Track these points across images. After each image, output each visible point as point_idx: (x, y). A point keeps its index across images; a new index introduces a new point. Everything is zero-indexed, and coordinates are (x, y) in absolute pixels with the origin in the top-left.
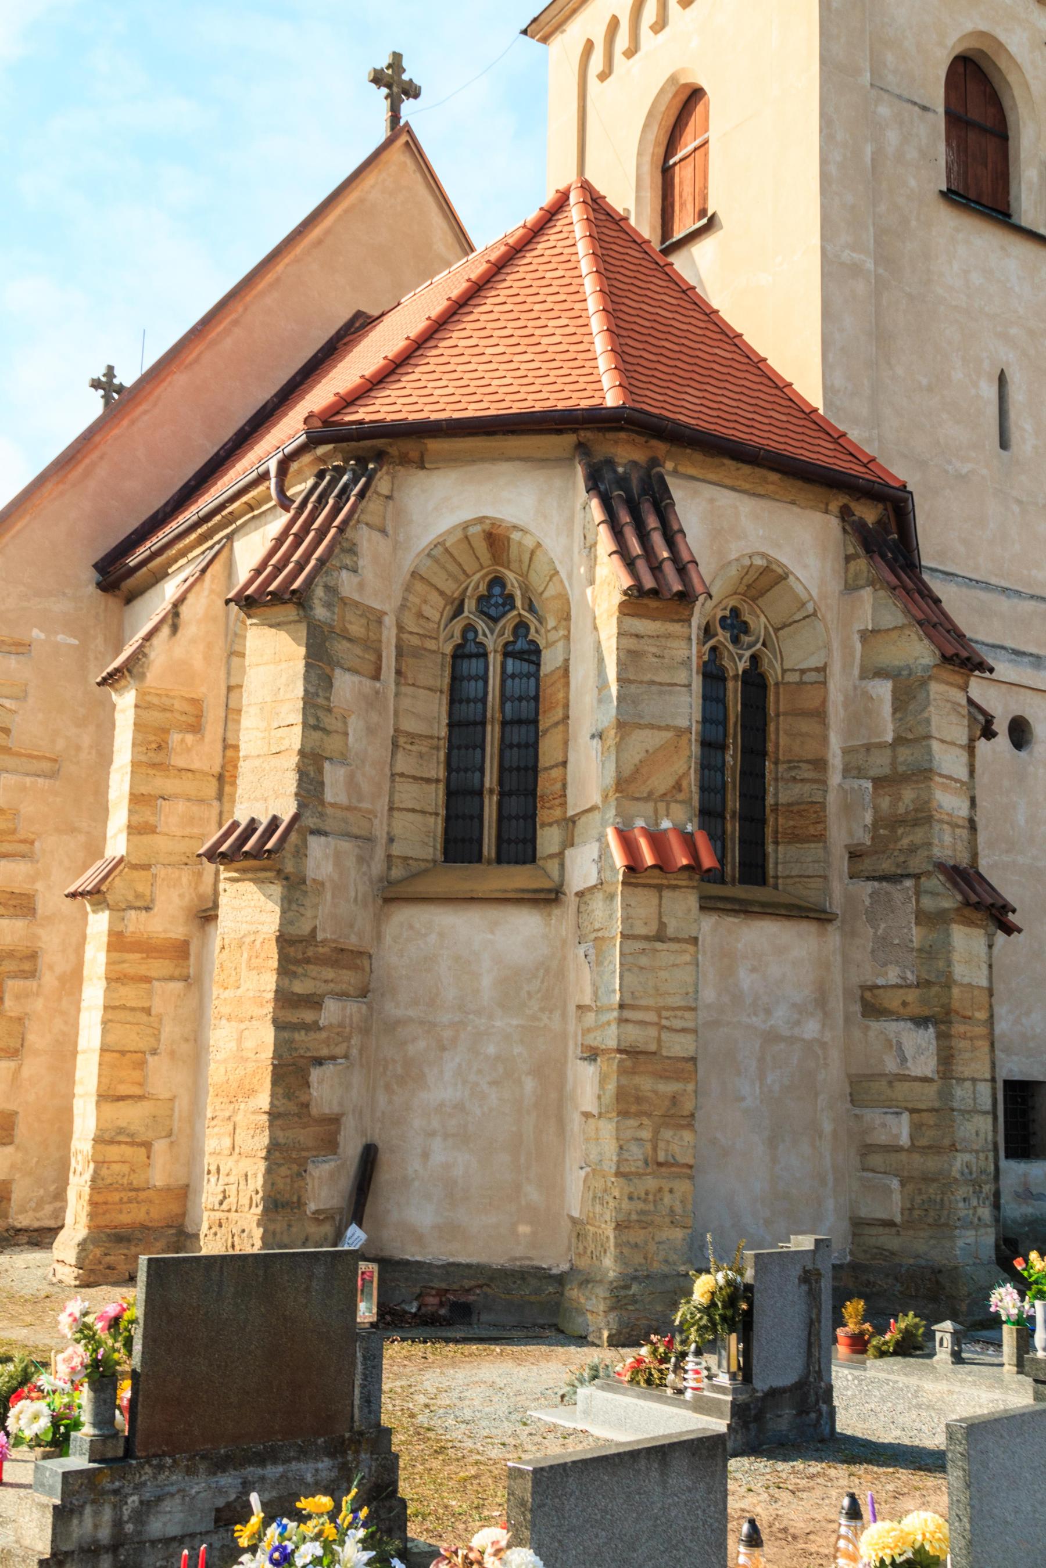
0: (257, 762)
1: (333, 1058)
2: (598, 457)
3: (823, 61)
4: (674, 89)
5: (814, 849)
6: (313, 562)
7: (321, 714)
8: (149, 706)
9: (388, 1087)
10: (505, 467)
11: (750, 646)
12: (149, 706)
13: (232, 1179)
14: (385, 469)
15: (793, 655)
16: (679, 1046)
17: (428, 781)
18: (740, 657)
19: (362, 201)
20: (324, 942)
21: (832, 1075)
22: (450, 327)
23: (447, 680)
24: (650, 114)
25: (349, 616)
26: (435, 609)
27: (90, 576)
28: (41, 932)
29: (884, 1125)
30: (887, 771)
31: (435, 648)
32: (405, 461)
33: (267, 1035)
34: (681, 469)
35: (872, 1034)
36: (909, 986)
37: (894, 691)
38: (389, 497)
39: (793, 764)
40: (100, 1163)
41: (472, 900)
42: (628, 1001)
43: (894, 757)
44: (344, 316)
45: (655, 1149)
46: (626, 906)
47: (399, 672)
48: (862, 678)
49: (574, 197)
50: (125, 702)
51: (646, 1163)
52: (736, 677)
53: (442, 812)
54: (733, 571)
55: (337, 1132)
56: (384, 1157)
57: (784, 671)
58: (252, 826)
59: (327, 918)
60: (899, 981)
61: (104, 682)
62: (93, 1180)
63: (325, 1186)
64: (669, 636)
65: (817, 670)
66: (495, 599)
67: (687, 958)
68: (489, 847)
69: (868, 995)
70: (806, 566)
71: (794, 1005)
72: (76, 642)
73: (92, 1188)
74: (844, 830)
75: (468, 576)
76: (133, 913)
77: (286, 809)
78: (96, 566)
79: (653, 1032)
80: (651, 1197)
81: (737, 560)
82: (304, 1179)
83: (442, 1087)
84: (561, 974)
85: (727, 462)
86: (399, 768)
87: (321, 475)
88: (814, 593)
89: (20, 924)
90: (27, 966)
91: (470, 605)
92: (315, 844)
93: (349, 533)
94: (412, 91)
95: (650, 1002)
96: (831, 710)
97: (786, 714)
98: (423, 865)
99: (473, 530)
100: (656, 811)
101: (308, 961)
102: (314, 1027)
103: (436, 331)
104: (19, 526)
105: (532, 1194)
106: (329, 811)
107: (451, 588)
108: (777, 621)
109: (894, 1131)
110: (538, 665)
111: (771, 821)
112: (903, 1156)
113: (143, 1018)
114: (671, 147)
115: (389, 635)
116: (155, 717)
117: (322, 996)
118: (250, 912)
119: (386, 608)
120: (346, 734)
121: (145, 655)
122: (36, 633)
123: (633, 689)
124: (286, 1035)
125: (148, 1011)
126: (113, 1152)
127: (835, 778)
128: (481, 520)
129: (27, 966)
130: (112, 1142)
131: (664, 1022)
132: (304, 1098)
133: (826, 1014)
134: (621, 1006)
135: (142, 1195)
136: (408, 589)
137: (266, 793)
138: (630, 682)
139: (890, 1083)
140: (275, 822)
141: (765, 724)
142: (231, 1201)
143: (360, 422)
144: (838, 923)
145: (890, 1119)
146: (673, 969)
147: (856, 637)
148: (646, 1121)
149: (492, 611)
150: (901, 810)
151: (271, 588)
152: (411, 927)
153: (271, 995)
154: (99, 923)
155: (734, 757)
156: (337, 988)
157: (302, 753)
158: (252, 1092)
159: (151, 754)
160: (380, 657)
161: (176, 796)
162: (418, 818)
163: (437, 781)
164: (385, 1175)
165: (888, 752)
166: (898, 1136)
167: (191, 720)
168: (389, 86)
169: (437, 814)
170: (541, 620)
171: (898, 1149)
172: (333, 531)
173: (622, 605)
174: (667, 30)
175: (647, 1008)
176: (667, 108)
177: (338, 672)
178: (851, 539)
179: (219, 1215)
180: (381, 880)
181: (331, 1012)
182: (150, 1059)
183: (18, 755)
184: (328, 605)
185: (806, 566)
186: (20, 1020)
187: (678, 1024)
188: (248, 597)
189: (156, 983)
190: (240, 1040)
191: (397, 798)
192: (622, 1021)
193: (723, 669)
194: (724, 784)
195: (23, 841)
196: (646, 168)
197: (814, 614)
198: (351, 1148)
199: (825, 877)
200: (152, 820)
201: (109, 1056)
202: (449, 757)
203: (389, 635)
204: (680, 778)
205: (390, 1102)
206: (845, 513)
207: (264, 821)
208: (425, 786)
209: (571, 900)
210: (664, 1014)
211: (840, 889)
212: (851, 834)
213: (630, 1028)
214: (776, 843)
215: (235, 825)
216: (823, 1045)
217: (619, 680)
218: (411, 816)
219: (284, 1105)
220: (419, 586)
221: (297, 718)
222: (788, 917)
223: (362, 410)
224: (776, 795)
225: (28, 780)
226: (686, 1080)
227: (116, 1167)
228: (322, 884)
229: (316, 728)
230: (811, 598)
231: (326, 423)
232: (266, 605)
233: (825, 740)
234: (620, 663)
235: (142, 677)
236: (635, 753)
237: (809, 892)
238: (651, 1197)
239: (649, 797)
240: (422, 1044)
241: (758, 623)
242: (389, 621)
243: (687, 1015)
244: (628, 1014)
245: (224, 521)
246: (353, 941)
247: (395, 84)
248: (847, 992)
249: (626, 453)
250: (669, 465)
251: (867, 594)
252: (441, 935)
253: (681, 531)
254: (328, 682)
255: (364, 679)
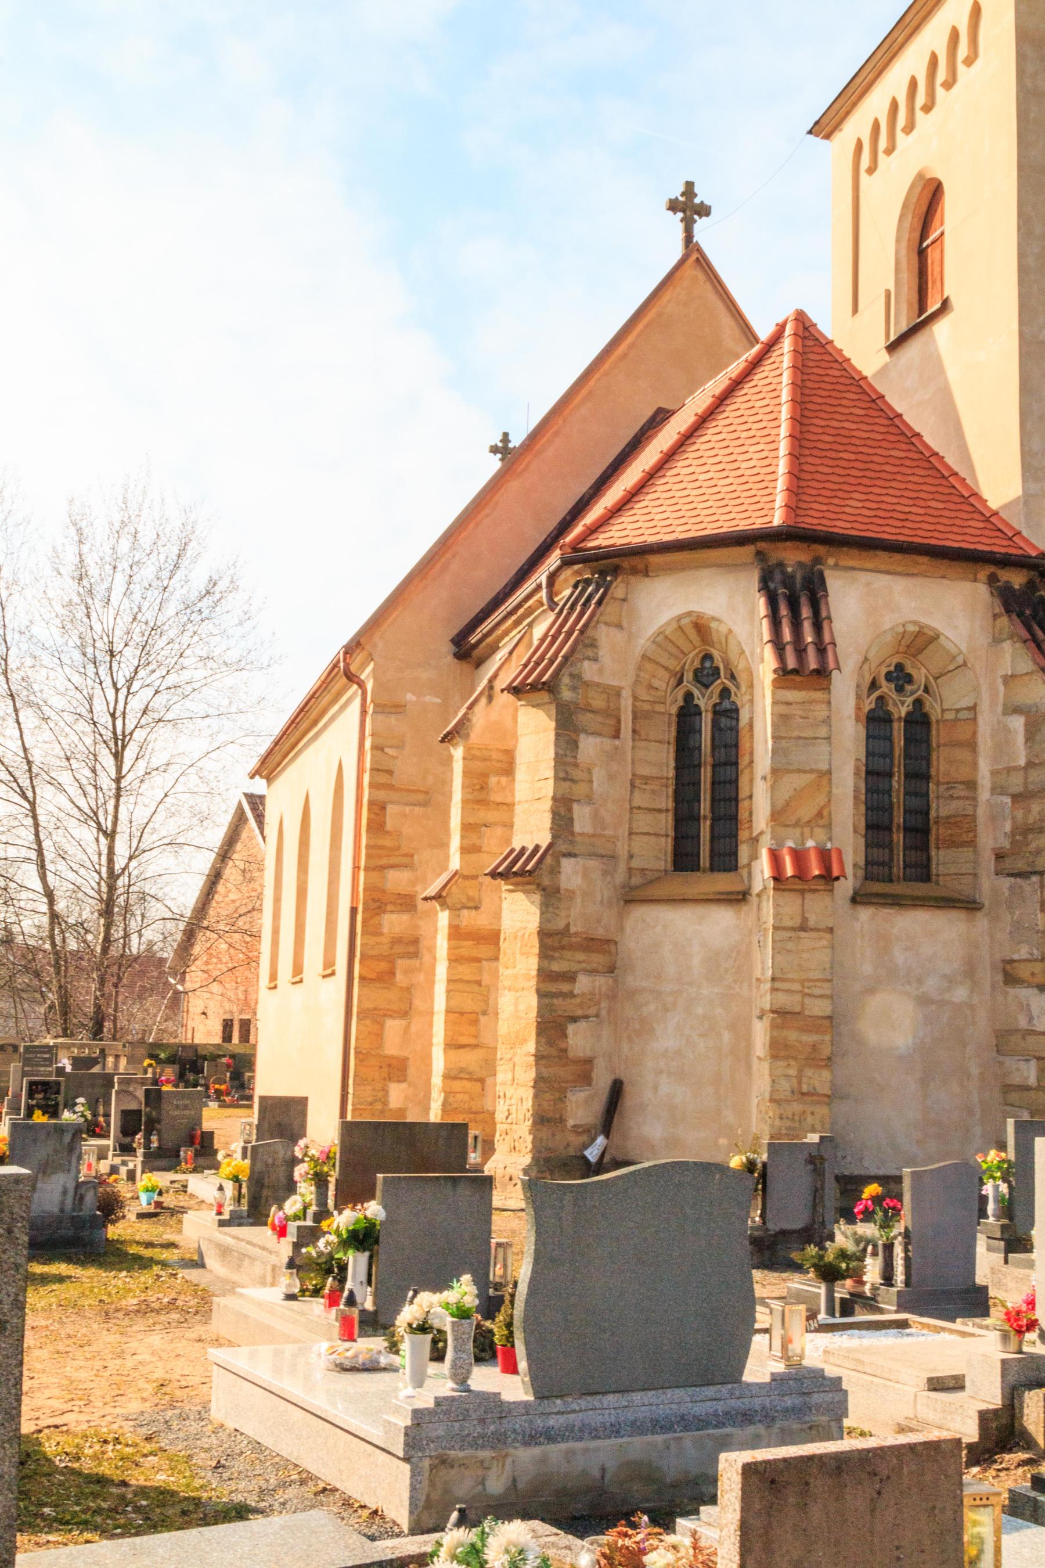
0: (526, 806)
1: (587, 1017)
2: (773, 561)
3: (1021, 167)
4: (922, 183)
5: (967, 853)
6: (559, 659)
7: (569, 769)
8: (474, 758)
9: (629, 1037)
10: (705, 572)
11: (913, 693)
12: (474, 758)
13: (513, 1101)
14: (619, 579)
15: (950, 698)
16: (820, 1008)
17: (660, 811)
18: (903, 703)
19: (660, 315)
20: (576, 934)
21: (981, 1029)
22: (676, 457)
23: (674, 734)
24: (905, 206)
25: (591, 694)
26: (662, 681)
27: (448, 648)
28: (421, 923)
29: (1018, 1070)
30: (1019, 789)
31: (663, 710)
32: (635, 571)
33: (533, 1001)
34: (842, 563)
35: (1010, 998)
36: (1036, 960)
37: (1026, 725)
38: (624, 600)
39: (950, 785)
40: (448, 1093)
41: (685, 901)
42: (778, 975)
43: (1026, 778)
44: (649, 413)
45: (800, 1083)
46: (776, 906)
47: (634, 731)
48: (1005, 713)
49: (789, 330)
50: (458, 753)
51: (793, 1092)
52: (900, 718)
53: (672, 833)
54: (888, 638)
55: (591, 1070)
56: (627, 1088)
57: (943, 711)
58: (523, 849)
59: (577, 917)
60: (1028, 957)
61: (442, 741)
62: (443, 1105)
63: (582, 1107)
64: (812, 702)
65: (968, 709)
66: (707, 672)
67: (824, 943)
68: (705, 859)
69: (1008, 967)
70: (955, 627)
71: (944, 976)
72: (438, 700)
73: (443, 1111)
74: (991, 837)
75: (685, 655)
76: (465, 912)
77: (544, 839)
78: (452, 641)
79: (798, 998)
80: (797, 1118)
81: (892, 629)
82: (564, 1102)
83: (667, 1038)
84: (748, 954)
85: (880, 553)
86: (637, 802)
87: (575, 587)
88: (964, 648)
89: (405, 917)
90: (411, 949)
91: (689, 676)
92: (567, 864)
93: (590, 632)
94: (704, 211)
95: (795, 976)
96: (980, 740)
97: (945, 745)
98: (656, 874)
99: (685, 621)
100: (802, 834)
101: (563, 948)
102: (571, 995)
103: (666, 462)
104: (394, 616)
105: (729, 1116)
106: (579, 839)
107: (673, 664)
108: (935, 671)
109: (1025, 1074)
110: (738, 720)
111: (934, 832)
112: (1032, 1094)
113: (476, 988)
114: (924, 235)
115: (626, 704)
116: (478, 765)
117: (576, 973)
118: (519, 914)
119: (623, 684)
120: (591, 781)
121: (469, 720)
122: (410, 697)
123: (784, 743)
124: (546, 1001)
125: (479, 983)
126: (457, 1085)
127: (984, 795)
128: (689, 614)
129: (411, 949)
130: (455, 1078)
131: (807, 991)
132: (563, 1046)
133: (974, 982)
134: (773, 979)
135: (480, 1117)
136: (640, 668)
137: (532, 829)
138: (783, 738)
139: (1023, 1037)
140: (537, 848)
141: (929, 754)
142: (513, 1116)
143: (599, 547)
144: (985, 910)
145: (1023, 1065)
146: (815, 954)
147: (1000, 681)
148: (792, 1062)
149: (705, 680)
150: (1031, 821)
151: (529, 681)
152: (644, 921)
153: (534, 973)
154: (443, 918)
155: (898, 782)
156: (589, 967)
157: (554, 799)
158: (524, 1041)
159: (476, 794)
160: (619, 721)
161: (495, 824)
162: (653, 839)
163: (667, 810)
164: (629, 1101)
165: (1022, 773)
166: (1027, 1078)
167: (505, 766)
168: (684, 211)
169: (667, 836)
170: (738, 687)
171: (1028, 1088)
172: (576, 633)
173: (774, 681)
174: (915, 132)
175: (792, 980)
176: (919, 199)
177: (582, 736)
178: (997, 602)
179: (505, 1126)
180: (623, 887)
181: (583, 984)
182: (481, 1018)
183: (400, 790)
184: (574, 688)
185: (955, 627)
186: (408, 989)
187: (817, 991)
188: (515, 688)
189: (485, 963)
190: (516, 1004)
191: (634, 825)
192: (774, 990)
193: (889, 714)
194: (891, 804)
195: (406, 855)
196: (903, 252)
197: (965, 664)
198: (602, 1082)
199: (975, 875)
200: (478, 842)
201: (452, 1016)
202: (676, 792)
203: (626, 704)
204: (822, 809)
205: (631, 1049)
206: (992, 579)
207: (531, 848)
208: (657, 815)
209: (754, 899)
210: (807, 984)
211: (990, 885)
212: (996, 839)
213: (780, 994)
214: (938, 848)
215: (512, 850)
216: (972, 1007)
217: (773, 737)
218: (646, 838)
219: (546, 1050)
220: (648, 666)
221: (550, 773)
222: (939, 907)
223: (602, 536)
224: (937, 810)
225: (407, 809)
226: (824, 1033)
227: (459, 1096)
228: (573, 892)
229: (565, 779)
230: (961, 653)
231: (575, 549)
232: (528, 692)
233: (975, 765)
234: (773, 725)
235: (467, 736)
236: (786, 791)
237: (963, 888)
238: (797, 1118)
239: (797, 824)
240: (652, 1007)
241: (920, 675)
242: (626, 694)
243: (826, 985)
244: (778, 985)
245: (522, 615)
246: (600, 933)
247: (688, 207)
248: (993, 965)
249: (793, 557)
250: (831, 561)
251: (1007, 645)
252: (665, 927)
253: (829, 618)
254: (575, 745)
255: (605, 740)
